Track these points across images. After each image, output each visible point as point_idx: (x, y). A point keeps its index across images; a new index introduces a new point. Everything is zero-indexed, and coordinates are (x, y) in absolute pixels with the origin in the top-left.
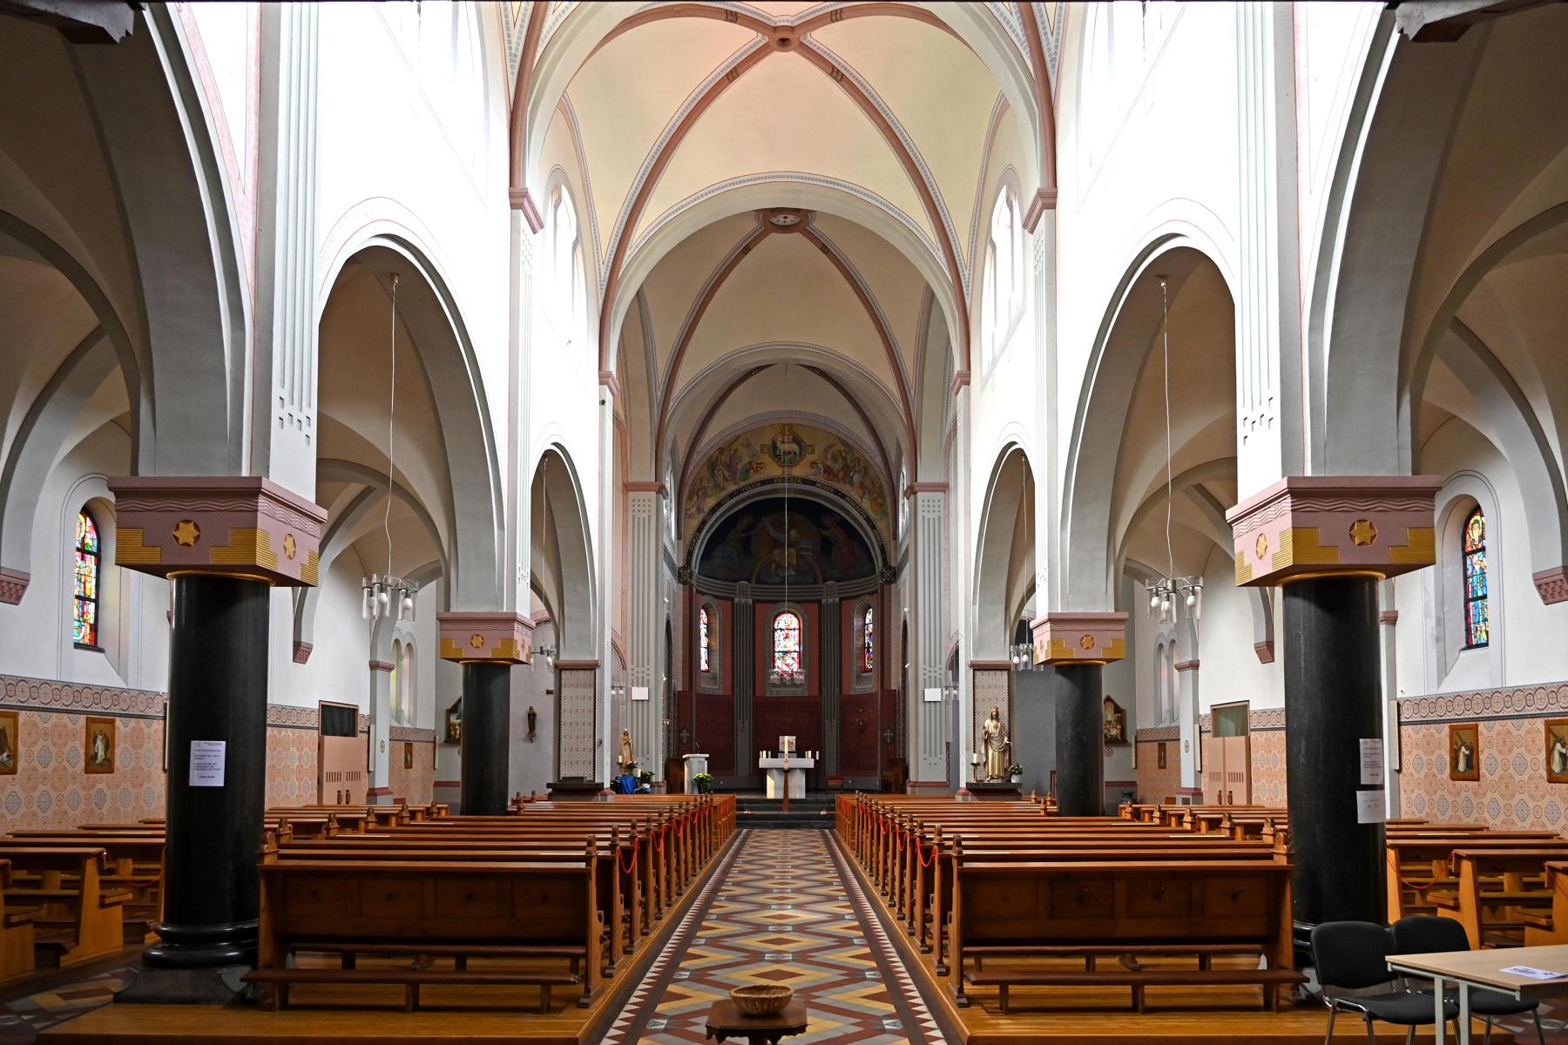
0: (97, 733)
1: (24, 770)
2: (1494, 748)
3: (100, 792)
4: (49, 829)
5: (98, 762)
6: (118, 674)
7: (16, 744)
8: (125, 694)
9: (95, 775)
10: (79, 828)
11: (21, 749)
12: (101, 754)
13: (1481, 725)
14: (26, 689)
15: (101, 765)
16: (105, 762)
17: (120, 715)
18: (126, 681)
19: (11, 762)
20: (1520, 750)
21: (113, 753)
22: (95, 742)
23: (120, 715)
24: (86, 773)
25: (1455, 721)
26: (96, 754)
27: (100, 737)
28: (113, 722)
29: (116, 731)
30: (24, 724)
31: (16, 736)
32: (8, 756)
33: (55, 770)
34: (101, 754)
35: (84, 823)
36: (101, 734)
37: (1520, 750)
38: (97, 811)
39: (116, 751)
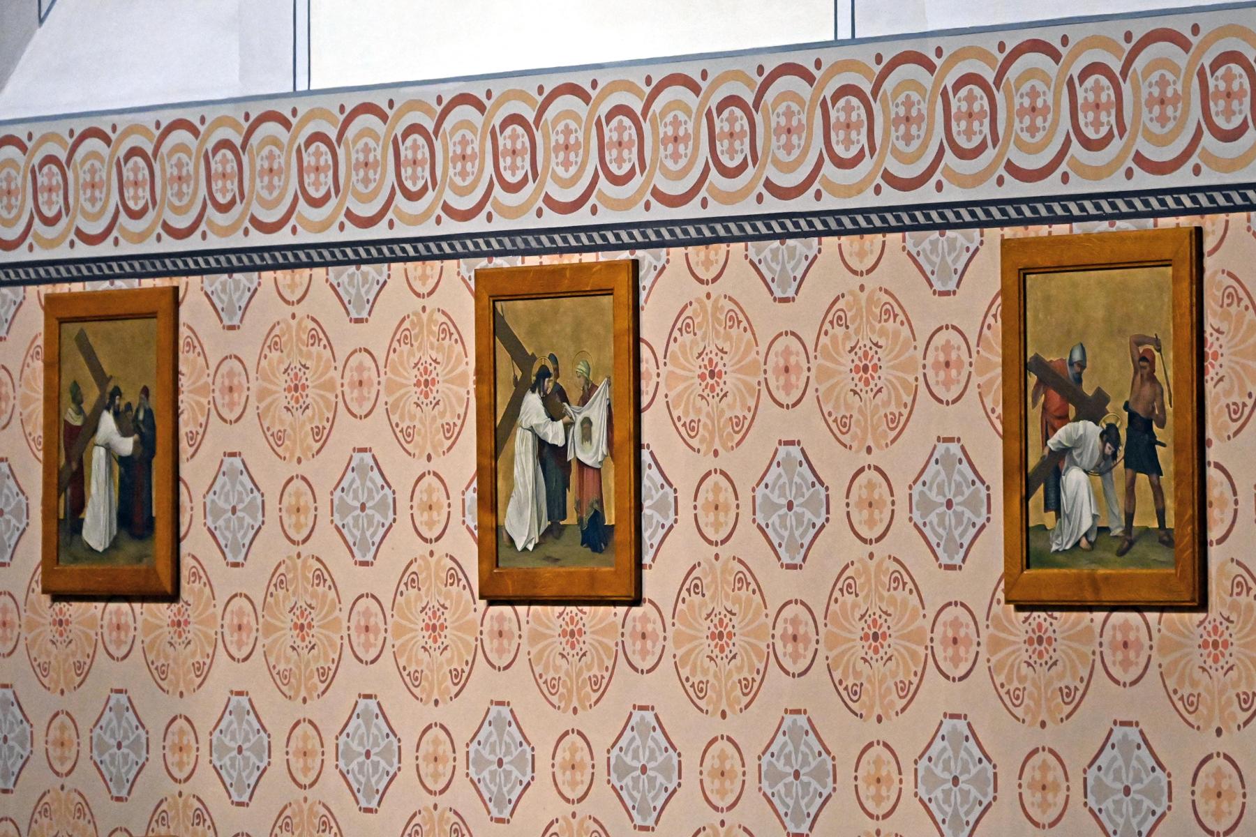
20: (368, 679)
24: (1201, 604)
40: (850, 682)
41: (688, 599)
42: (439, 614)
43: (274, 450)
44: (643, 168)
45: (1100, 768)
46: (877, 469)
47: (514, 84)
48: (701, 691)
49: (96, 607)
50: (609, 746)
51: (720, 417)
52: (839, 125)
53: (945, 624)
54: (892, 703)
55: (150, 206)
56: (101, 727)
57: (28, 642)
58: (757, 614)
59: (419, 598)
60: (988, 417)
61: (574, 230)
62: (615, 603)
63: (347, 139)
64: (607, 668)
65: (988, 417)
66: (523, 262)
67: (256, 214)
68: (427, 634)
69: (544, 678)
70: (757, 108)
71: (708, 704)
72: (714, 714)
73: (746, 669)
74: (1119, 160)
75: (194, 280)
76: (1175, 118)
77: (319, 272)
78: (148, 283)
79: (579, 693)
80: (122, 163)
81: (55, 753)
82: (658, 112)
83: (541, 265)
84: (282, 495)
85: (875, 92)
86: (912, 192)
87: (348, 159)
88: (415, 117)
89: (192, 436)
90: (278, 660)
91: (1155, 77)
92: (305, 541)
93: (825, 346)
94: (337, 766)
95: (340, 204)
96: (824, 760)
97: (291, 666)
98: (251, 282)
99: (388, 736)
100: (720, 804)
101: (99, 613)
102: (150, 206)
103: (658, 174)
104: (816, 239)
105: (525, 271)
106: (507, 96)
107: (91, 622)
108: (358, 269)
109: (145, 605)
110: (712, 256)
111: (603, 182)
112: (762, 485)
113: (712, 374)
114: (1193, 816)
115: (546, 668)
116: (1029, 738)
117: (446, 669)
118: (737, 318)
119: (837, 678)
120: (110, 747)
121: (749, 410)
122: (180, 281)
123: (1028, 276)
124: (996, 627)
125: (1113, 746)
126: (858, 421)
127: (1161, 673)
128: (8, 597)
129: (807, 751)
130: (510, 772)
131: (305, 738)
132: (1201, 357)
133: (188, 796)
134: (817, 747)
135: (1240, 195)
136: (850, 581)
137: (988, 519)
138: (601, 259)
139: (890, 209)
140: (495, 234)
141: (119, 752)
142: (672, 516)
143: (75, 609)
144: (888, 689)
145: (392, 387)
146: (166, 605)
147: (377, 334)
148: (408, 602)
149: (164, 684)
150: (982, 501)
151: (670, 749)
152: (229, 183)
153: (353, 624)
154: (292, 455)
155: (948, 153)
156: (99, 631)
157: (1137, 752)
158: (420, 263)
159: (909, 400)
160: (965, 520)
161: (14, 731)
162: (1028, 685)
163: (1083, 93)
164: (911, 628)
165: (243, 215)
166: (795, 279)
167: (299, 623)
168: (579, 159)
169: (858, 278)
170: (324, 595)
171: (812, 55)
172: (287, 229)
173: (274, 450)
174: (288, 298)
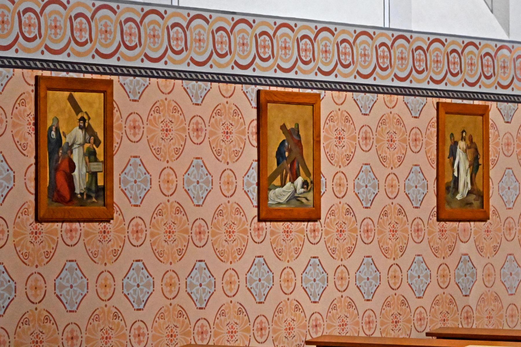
0: (457, 137)
1: (331, 212)
2: (425, 242)
3: (465, 258)
4: (377, 334)
5: (459, 197)
6: (492, 11)
7: (317, 161)
8: (505, 51)
9: (455, 224)
10: (428, 334)
11: (325, 167)
12: (464, 179)
13: (327, 96)
14: (292, 44)
15: (465, 203)
16: (473, 197)
17: (498, 98)
18: (508, 34)
19: (310, 196)
20: (201, 254)
21: (486, 178)
22: (453, 154)
23: (498, 98)
24: (439, 220)
25: (45, 65)
26: (456, 180)
27: (462, 145)
28: (484, 112)
29: (491, 131)
30: (330, 118)
31: (317, 142)
32: (305, 184)
33: (159, 211)
34: (464, 179)
35: (437, 326)
36: (463, 139)
37: (201, 254)
38: (461, 302)
39: (492, 173)
40: (278, 248)
41: (21, 217)
42: (232, 227)
43: (156, 157)
44: (314, 60)
45: (306, 273)
46: (231, 170)
47: (489, 42)
48: (95, 254)
49: (58, 225)
50: (186, 277)
51: (342, 155)
52: (343, 53)
53: (196, 227)
54: (447, 253)
55: (89, 41)
56: (191, 277)
57: (326, 240)
58: (121, 223)
59: (387, 220)
60: (151, 149)
61: (473, 93)
62: (304, 221)
63: (191, 28)
64: (244, 246)
65: (151, 149)
66: (84, 76)
67: (320, 67)
68: (226, 234)
69: (157, 251)
70: (274, 37)
71: (164, 259)
72: (338, 260)
73: (296, 244)
74: (139, 55)
75: (328, 93)
76: (7, 29)
77: (349, 94)
78: (476, 102)
79: (289, 255)
80: (22, 15)
81: (166, 289)
82: (146, 23)
83: (277, 91)
84: (160, 175)
85: (42, 12)
86: (56, 56)
87: (191, 37)
88: (80, 10)
89: (493, 160)
90: (383, 244)
91: (151, 27)
92: (343, 197)
93: (151, 120)
94: (186, 291)
95: (392, 71)
96: (149, 280)
97: (439, 245)
98: (423, 101)
99: (148, 277)
100: (169, 297)
101: (457, 226)
102: (89, 41)
103: (358, 66)
104: (210, 83)
105: (474, 105)
106: (418, 39)
107: (302, 231)
108: (134, 78)
109: (272, 223)
110: (341, 95)
111: (257, 60)
112: (247, 176)
113: (391, 141)
114: (223, 291)
115: (277, 245)
116: (485, 261)
117: (175, 249)
118: (348, 119)
119: (477, 244)
120: (196, 286)
121: (241, 148)
122: (489, 103)
123: (102, 94)
124: (215, 228)
125: (196, 269)
126: (337, 156)
127: (14, 244)
128: (201, 220)
129: (142, 276)
130: (205, 289)
131: (106, 279)
132: (36, 124)
133: (292, 300)
134: (80, 275)
135: (78, 66)
136: (26, 210)
137: (151, 188)
138: (453, 102)
139: (279, 78)
140: (481, 93)
141: (465, 278)
142: (149, 186)
143: (46, 226)
144: (234, 251)
145: (354, 138)
146: (98, 223)
147: (205, 111)
148: (384, 221)
149: (482, 254)
150: (186, 182)
151: (150, 277)
152: (224, 46)
153: (362, 230)
154: (165, 159)
155: (214, 55)
156: (190, 235)
157: (318, 267)
158: (164, 80)
159: (183, 144)
160: (203, 189)
161: (319, 277)
162: (337, 247)
163: (302, 44)
164: (184, 227)
165: (354, 70)
166: (139, 93)
167: (229, 230)
168: (248, 49)
169: (338, 106)
170: (402, 219)
171: (334, 26)
172: (115, 58)
173: (156, 157)
174: (225, 95)
